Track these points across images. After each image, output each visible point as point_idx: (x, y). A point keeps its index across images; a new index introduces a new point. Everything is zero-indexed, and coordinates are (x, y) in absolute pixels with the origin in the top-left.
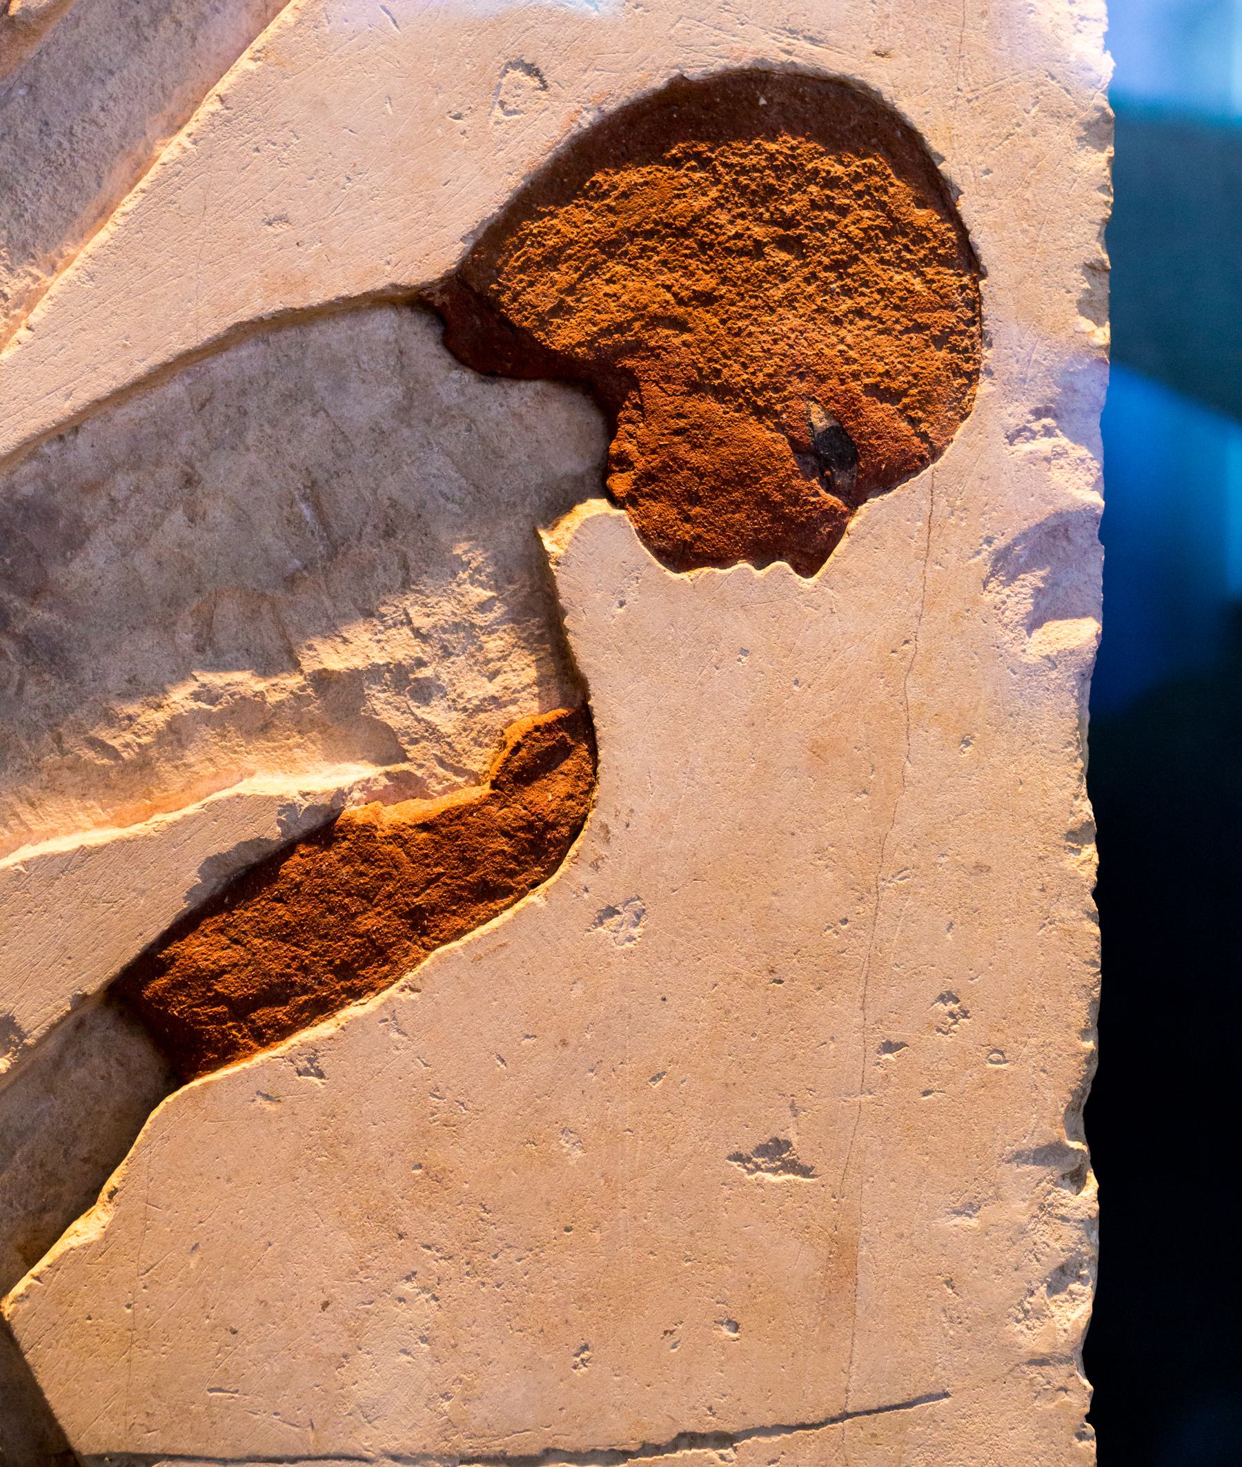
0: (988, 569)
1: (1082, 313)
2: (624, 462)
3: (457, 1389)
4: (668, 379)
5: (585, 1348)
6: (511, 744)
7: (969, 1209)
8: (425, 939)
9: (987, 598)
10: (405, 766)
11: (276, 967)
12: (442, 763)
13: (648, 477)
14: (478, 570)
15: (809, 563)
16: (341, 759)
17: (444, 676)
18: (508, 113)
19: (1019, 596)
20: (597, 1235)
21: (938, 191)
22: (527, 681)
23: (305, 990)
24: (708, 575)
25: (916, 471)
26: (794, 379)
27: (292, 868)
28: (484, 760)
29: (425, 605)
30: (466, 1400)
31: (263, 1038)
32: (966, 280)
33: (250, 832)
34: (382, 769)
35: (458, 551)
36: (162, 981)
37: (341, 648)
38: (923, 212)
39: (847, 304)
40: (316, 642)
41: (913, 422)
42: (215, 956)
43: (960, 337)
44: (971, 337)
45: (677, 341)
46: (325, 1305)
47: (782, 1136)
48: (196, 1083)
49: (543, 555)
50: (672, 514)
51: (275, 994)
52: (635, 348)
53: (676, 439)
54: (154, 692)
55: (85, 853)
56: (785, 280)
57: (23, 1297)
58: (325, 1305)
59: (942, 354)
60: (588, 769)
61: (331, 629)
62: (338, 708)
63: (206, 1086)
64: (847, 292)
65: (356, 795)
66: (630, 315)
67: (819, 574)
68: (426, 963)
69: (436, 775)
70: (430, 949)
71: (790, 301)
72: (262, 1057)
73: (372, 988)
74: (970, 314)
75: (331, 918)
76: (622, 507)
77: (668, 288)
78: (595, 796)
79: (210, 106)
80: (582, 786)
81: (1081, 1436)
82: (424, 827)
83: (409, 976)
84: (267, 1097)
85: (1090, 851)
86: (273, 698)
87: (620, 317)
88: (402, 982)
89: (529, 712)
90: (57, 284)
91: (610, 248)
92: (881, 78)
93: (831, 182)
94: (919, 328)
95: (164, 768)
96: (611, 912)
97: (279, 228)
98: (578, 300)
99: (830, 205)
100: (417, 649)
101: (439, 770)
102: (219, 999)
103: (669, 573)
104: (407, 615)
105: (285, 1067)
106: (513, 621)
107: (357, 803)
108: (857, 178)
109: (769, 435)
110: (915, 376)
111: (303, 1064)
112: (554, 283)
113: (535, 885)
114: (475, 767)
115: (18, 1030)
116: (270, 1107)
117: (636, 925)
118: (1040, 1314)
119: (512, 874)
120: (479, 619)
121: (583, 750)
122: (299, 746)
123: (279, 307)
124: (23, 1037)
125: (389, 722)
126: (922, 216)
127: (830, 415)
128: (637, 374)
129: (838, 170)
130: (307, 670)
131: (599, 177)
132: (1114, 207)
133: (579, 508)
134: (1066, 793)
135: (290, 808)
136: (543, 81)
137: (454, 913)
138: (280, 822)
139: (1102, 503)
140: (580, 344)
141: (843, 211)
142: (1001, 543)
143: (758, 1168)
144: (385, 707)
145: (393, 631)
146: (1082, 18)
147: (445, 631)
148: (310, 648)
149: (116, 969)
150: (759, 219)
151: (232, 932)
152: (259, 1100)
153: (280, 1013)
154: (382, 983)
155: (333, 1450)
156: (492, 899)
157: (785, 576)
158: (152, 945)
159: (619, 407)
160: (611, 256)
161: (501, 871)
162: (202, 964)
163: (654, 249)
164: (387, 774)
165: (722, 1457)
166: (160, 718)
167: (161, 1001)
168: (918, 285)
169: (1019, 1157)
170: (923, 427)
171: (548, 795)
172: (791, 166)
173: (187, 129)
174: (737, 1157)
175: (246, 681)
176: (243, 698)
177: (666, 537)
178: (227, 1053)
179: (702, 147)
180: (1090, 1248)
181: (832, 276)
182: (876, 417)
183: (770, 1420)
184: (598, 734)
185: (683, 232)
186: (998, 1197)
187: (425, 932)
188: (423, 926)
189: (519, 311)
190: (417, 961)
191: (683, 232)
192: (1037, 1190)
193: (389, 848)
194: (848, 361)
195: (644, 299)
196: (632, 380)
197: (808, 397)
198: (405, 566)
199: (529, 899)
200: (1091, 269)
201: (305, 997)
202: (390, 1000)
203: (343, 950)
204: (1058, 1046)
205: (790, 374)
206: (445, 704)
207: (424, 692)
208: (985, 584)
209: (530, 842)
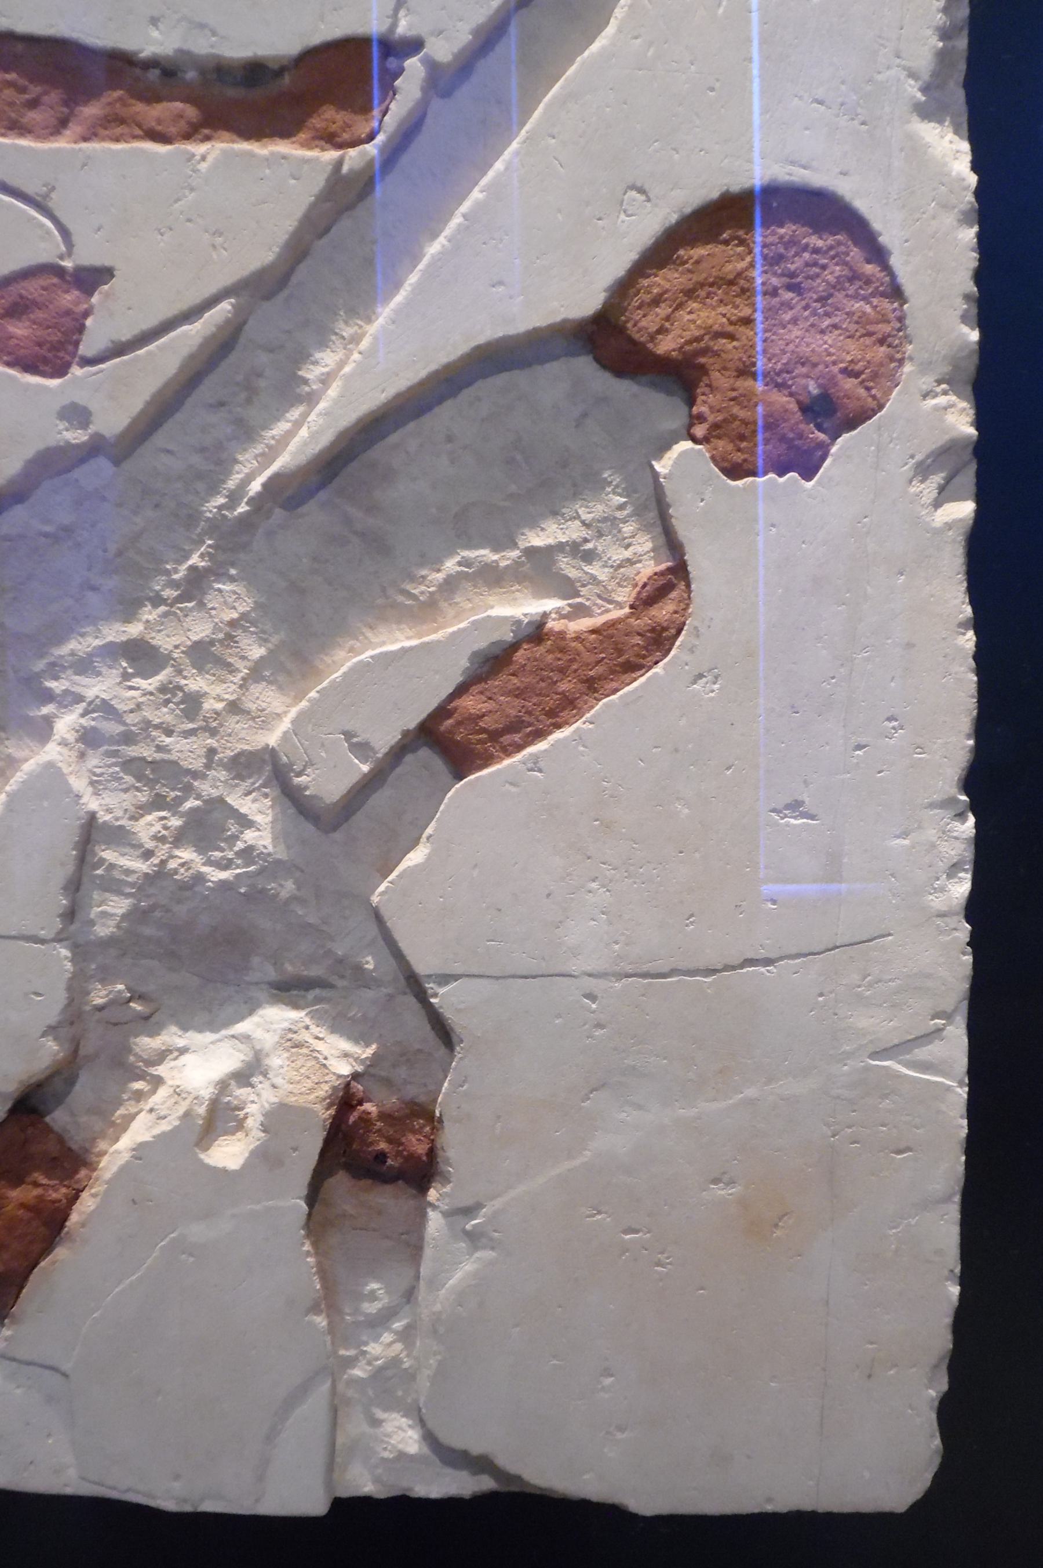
0: (912, 473)
1: (963, 322)
2: (700, 418)
3: (623, 938)
4: (725, 368)
5: (692, 915)
6: (640, 584)
7: (905, 835)
8: (596, 695)
9: (912, 490)
10: (579, 600)
11: (513, 712)
12: (599, 596)
13: (716, 426)
14: (617, 486)
15: (808, 473)
16: (543, 598)
17: (599, 548)
18: (628, 216)
19: (929, 489)
20: (697, 855)
21: (878, 254)
22: (646, 549)
23: (530, 725)
24: (752, 482)
25: (870, 418)
26: (799, 366)
27: (520, 656)
28: (625, 595)
29: (587, 507)
30: (627, 945)
31: (508, 751)
32: (896, 305)
33: (495, 637)
34: (566, 602)
35: (605, 475)
36: (450, 722)
37: (541, 533)
38: (869, 266)
39: (827, 322)
40: (526, 531)
41: (868, 389)
42: (479, 706)
43: (890, 337)
44: (900, 339)
45: (730, 346)
46: (549, 895)
47: (800, 798)
48: (472, 777)
49: (655, 475)
50: (730, 447)
51: (513, 727)
52: (705, 351)
53: (732, 403)
54: (436, 564)
55: (404, 651)
56: (792, 308)
57: (382, 894)
58: (549, 895)
59: (883, 349)
60: (686, 595)
61: (534, 523)
62: (540, 570)
63: (477, 778)
64: (827, 315)
65: (553, 616)
66: (702, 332)
67: (816, 479)
68: (597, 707)
69: (597, 605)
70: (599, 700)
71: (794, 321)
72: (507, 762)
73: (567, 723)
74: (899, 325)
75: (543, 684)
76: (701, 444)
77: (724, 315)
78: (690, 610)
79: (457, 220)
80: (682, 606)
81: (964, 954)
82: (593, 631)
83: (588, 715)
84: (511, 784)
85: (971, 634)
86: (503, 564)
87: (697, 333)
88: (584, 719)
89: (648, 568)
90: (372, 329)
91: (689, 294)
92: (845, 188)
93: (816, 251)
94: (870, 334)
95: (443, 605)
96: (701, 676)
97: (501, 289)
98: (672, 325)
99: (815, 264)
100: (584, 533)
101: (599, 602)
102: (483, 730)
103: (729, 481)
104: (577, 513)
105: (521, 767)
106: (638, 515)
107: (554, 620)
108: (831, 248)
109: (785, 399)
110: (868, 362)
111: (530, 765)
112: (657, 315)
113: (656, 663)
114: (619, 599)
115: (372, 749)
116: (513, 789)
117: (715, 683)
118: (942, 889)
119: (644, 657)
120: (619, 514)
121: (682, 585)
122: (518, 591)
123: (501, 334)
124: (375, 753)
125: (570, 575)
126: (869, 269)
127: (819, 386)
128: (707, 366)
129: (820, 243)
130: (522, 547)
131: (681, 252)
132: (980, 260)
133: (675, 447)
134: (958, 601)
135: (518, 622)
136: (647, 196)
137: (612, 680)
138: (512, 631)
139: (976, 433)
140: (674, 350)
141: (824, 267)
142: (919, 457)
143: (786, 816)
144: (567, 566)
145: (570, 523)
146: (958, 152)
147: (599, 521)
148: (523, 534)
149: (423, 716)
150: (775, 274)
151: (488, 694)
152: (507, 785)
153: (517, 737)
154: (573, 720)
155: (556, 972)
156: (633, 672)
157: (796, 481)
158: (444, 701)
159: (697, 386)
160: (690, 298)
161: (638, 655)
162: (473, 711)
163: (715, 293)
164: (569, 605)
165: (768, 971)
166: (440, 576)
167: (450, 732)
168: (868, 309)
169: (932, 806)
170: (874, 392)
171: (663, 612)
172: (792, 242)
173: (444, 234)
174: (774, 811)
175: (486, 554)
176: (486, 564)
177: (727, 460)
178: (487, 760)
179: (741, 233)
180: (969, 855)
181: (819, 305)
182: (847, 386)
183: (794, 951)
184: (691, 576)
185: (731, 283)
186: (919, 827)
187: (596, 691)
188: (593, 687)
189: (638, 332)
190: (592, 707)
191: (731, 283)
192: (942, 823)
193: (573, 644)
194: (829, 354)
195: (710, 322)
196: (703, 370)
197: (807, 376)
198: (575, 485)
199: (653, 671)
200: (967, 297)
201: (530, 729)
202: (578, 729)
203: (550, 702)
204: (954, 745)
205: (796, 363)
206: (600, 564)
207: (589, 557)
208: (911, 481)
209: (653, 638)
